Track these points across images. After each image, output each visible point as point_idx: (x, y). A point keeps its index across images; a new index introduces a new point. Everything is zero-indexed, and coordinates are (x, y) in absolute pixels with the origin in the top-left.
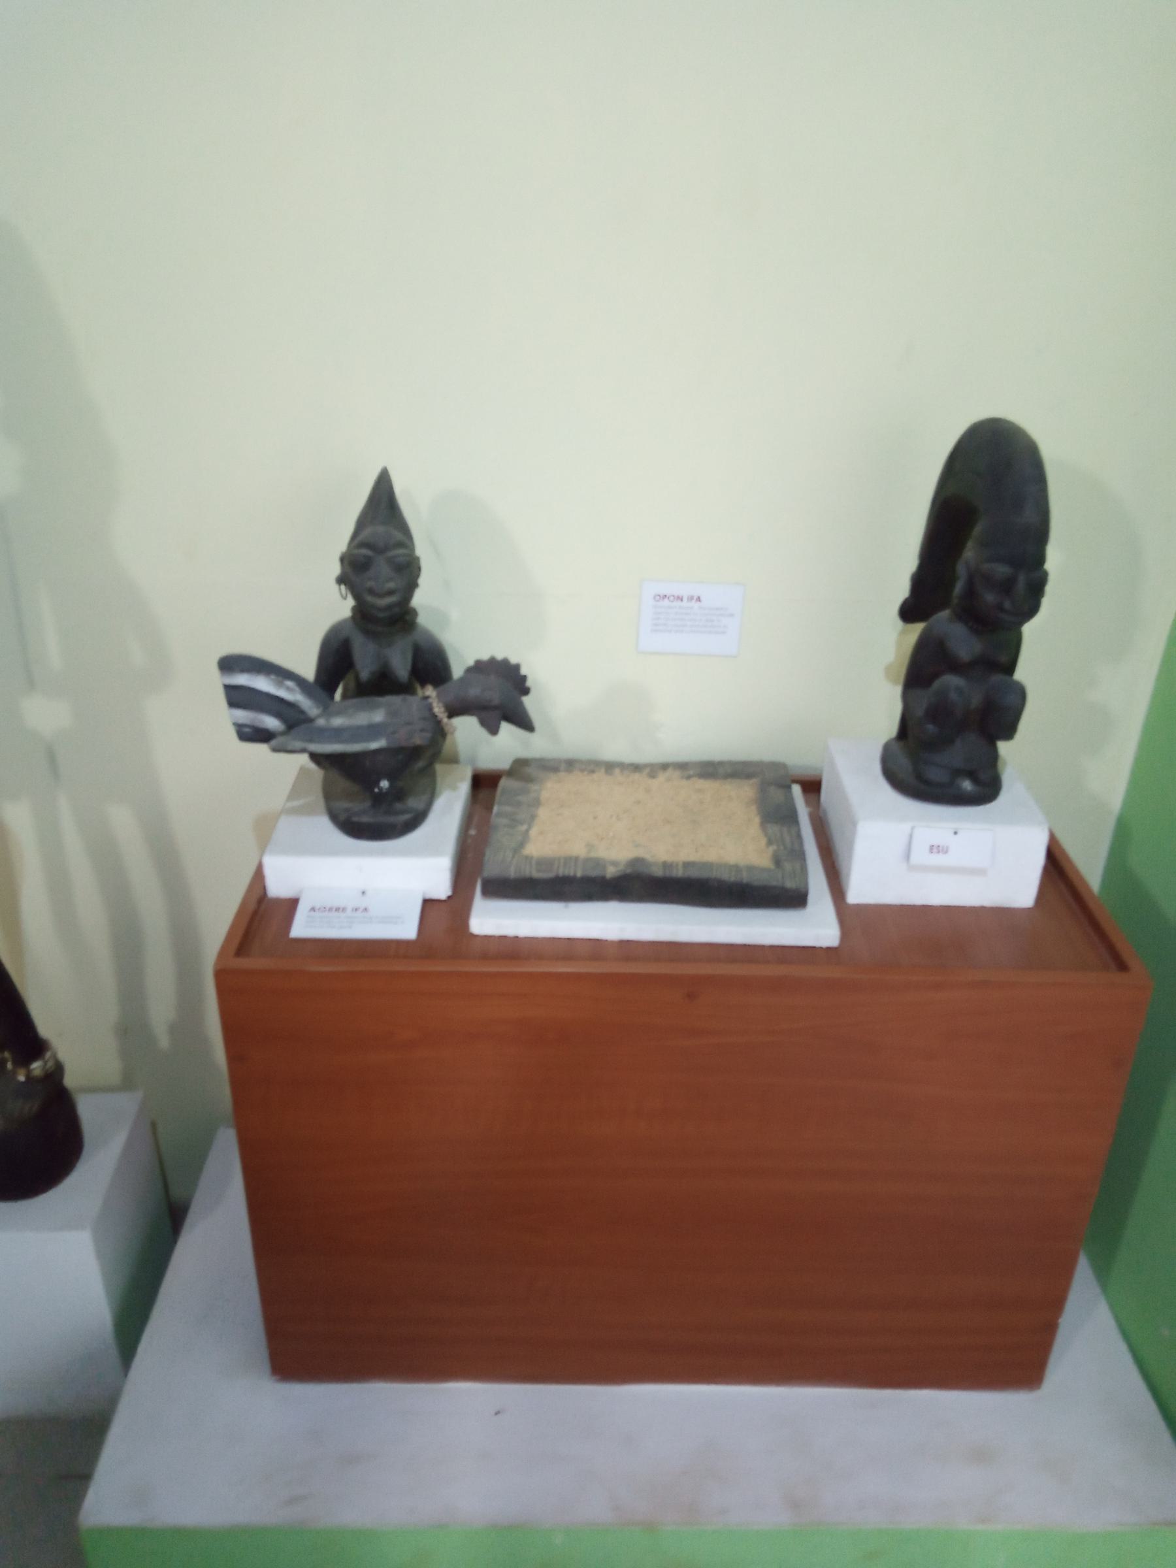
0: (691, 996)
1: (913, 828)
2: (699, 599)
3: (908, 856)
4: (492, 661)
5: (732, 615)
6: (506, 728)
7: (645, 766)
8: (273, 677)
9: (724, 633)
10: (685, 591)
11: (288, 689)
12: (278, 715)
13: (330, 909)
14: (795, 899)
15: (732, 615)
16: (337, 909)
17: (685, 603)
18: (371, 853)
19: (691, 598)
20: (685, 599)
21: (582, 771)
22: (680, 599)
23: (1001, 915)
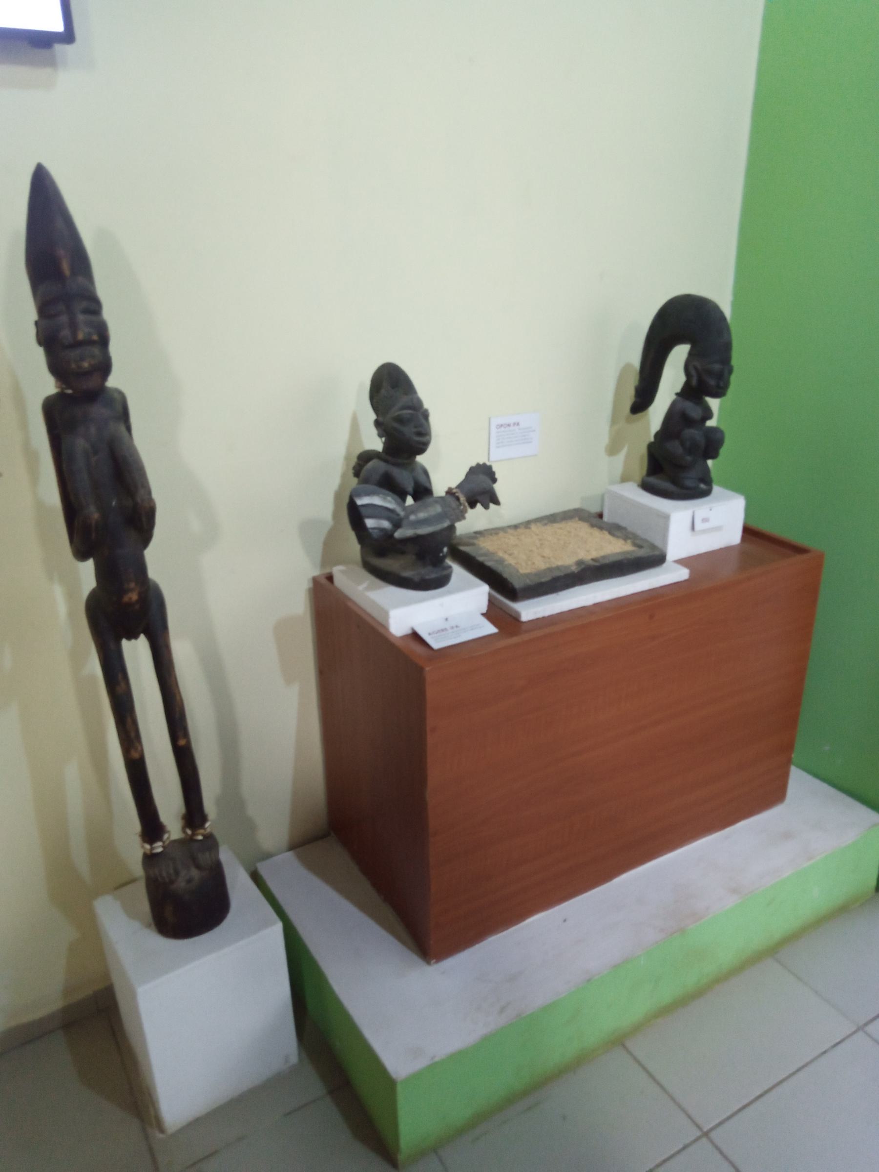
0: (651, 617)
1: (694, 513)
2: (518, 424)
3: (693, 528)
4: (478, 465)
5: (534, 431)
6: (492, 505)
7: (521, 524)
8: (381, 495)
9: (531, 442)
10: (511, 420)
11: (390, 502)
12: (388, 519)
13: (439, 631)
14: (656, 560)
15: (534, 431)
16: (443, 630)
17: (512, 428)
18: (433, 598)
19: (514, 424)
20: (512, 425)
21: (491, 534)
22: (509, 425)
23: (727, 550)
